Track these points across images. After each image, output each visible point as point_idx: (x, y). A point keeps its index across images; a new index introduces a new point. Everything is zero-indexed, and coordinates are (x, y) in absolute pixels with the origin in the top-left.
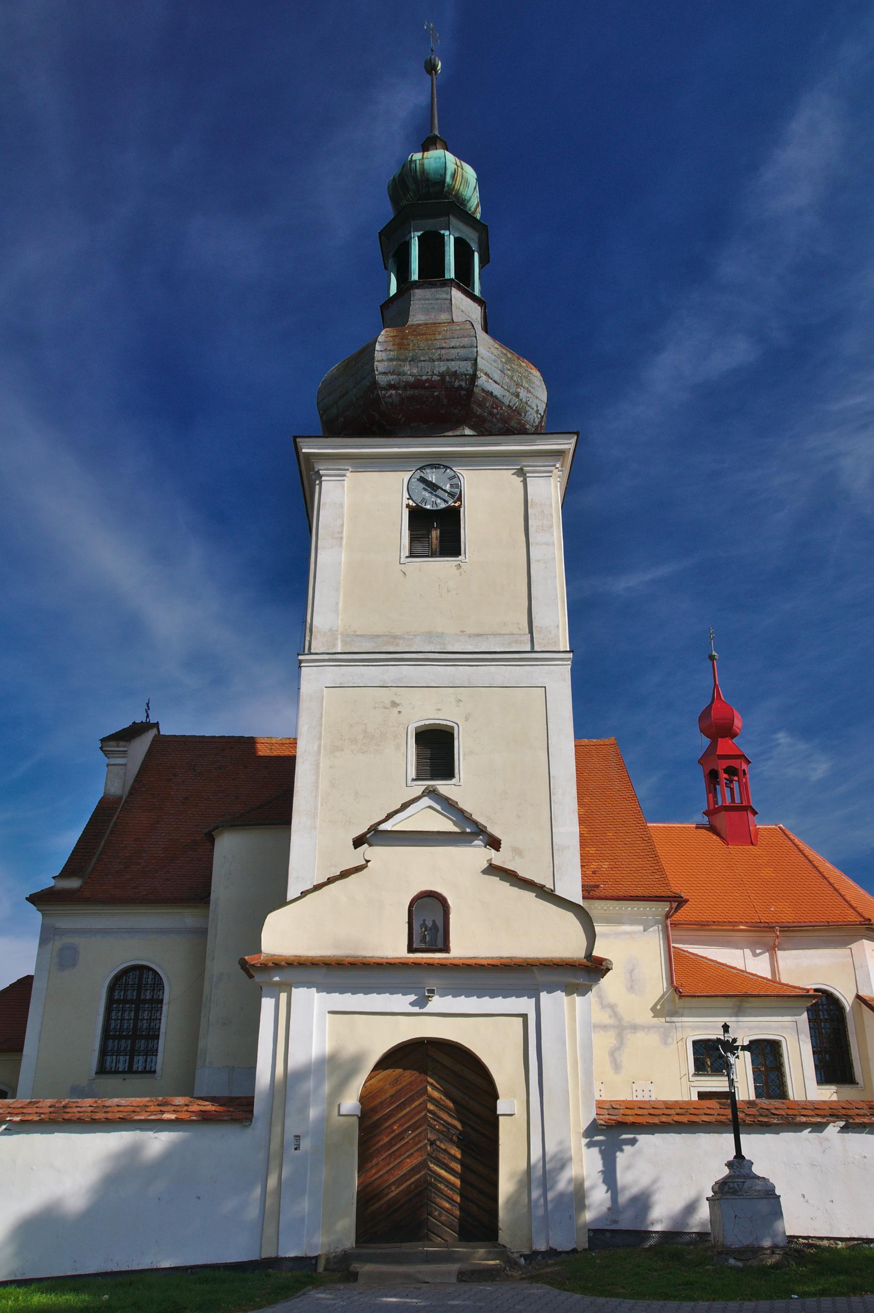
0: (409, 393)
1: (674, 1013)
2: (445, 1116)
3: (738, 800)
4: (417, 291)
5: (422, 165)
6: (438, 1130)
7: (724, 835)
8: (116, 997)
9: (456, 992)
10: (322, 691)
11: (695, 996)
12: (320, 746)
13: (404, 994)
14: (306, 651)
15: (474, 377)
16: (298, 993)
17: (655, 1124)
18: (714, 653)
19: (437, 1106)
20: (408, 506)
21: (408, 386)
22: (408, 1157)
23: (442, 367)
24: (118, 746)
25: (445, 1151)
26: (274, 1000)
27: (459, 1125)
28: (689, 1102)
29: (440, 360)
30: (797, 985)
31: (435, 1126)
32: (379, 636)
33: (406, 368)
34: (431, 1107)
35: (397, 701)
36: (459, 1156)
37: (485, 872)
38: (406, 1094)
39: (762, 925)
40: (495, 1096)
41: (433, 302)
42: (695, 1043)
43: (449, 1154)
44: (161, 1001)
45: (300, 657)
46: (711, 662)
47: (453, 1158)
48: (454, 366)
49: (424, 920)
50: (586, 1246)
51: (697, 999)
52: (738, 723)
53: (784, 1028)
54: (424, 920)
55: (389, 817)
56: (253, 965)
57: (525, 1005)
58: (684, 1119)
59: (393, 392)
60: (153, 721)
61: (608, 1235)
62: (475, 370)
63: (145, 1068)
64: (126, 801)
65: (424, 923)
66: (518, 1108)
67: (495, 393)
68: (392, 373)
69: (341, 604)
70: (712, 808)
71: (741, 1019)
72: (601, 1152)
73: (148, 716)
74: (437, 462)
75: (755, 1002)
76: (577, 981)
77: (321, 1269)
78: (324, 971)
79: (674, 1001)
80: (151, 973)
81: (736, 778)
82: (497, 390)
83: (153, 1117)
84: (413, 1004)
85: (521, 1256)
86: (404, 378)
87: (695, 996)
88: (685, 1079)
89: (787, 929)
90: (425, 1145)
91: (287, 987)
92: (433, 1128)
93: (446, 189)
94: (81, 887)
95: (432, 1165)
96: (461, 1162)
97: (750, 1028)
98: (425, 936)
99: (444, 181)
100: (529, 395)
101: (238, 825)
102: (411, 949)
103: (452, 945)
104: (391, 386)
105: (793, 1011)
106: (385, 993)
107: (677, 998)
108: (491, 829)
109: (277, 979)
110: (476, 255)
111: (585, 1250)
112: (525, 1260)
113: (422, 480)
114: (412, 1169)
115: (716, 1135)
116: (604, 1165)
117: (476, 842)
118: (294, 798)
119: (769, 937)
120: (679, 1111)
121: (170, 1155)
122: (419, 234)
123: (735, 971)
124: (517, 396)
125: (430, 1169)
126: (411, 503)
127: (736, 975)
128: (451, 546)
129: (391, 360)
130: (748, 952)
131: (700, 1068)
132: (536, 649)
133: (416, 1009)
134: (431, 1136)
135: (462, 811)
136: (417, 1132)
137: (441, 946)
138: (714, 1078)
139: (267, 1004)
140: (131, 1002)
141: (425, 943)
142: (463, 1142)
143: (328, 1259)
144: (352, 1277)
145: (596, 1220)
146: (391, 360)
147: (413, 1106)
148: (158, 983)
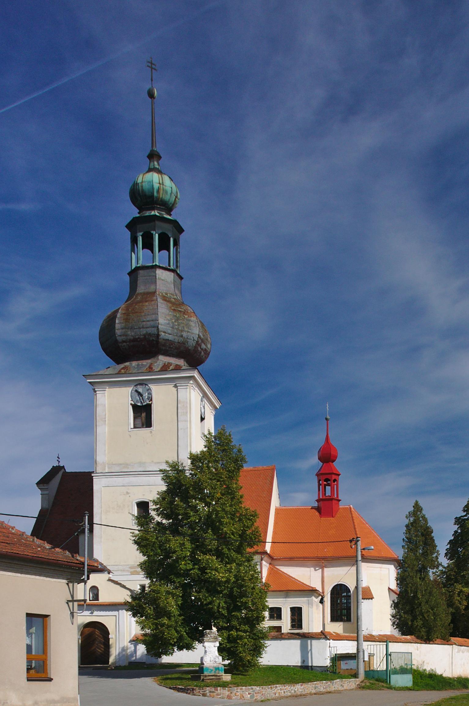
0: (132, 344)
3: (321, 497)
4: (140, 271)
5: (142, 186)
15: (158, 335)
20: (131, 404)
21: (131, 341)
23: (144, 331)
29: (143, 327)
32: (121, 464)
33: (129, 333)
40: (109, 634)
41: (148, 278)
46: (326, 421)
48: (150, 330)
59: (125, 344)
62: (158, 332)
67: (170, 339)
68: (124, 335)
69: (106, 452)
74: (142, 383)
75: (292, 593)
82: (170, 337)
86: (129, 338)
89: (325, 559)
93: (155, 199)
99: (153, 196)
100: (189, 334)
103: (100, 599)
104: (124, 342)
110: (172, 239)
113: (136, 391)
122: (141, 234)
124: (182, 336)
126: (133, 403)
128: (148, 423)
129: (122, 329)
130: (312, 569)
146: (122, 329)
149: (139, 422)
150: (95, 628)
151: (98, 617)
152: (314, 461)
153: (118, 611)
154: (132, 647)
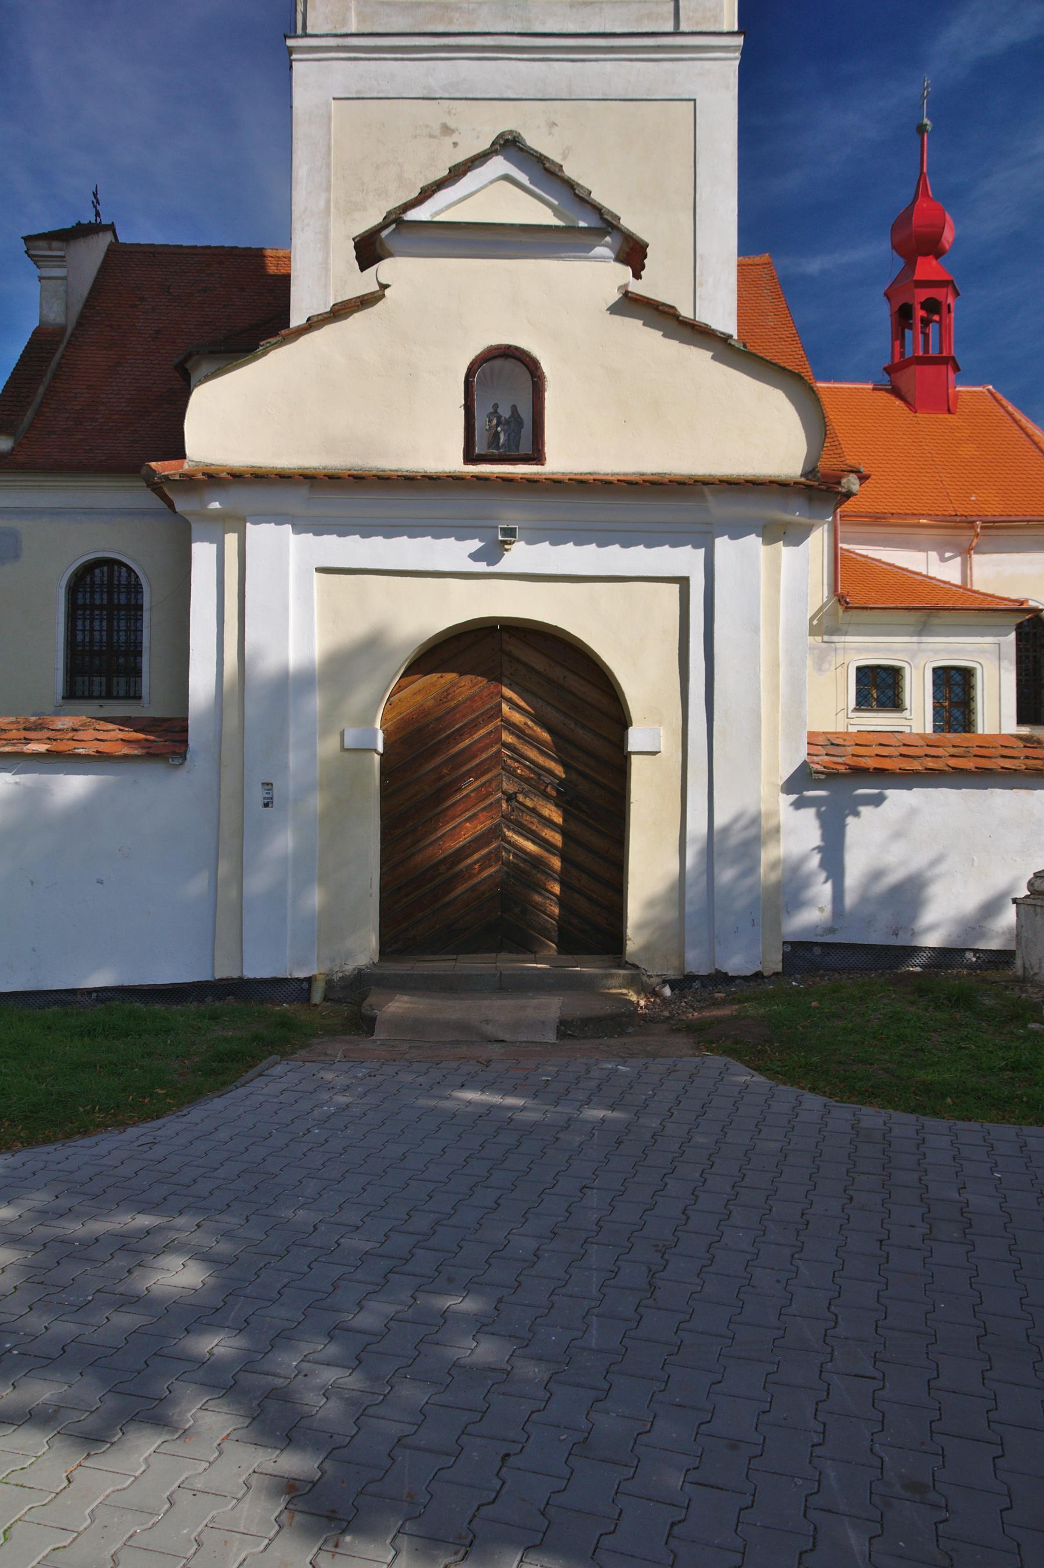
1: (834, 631)
2: (532, 754)
6: (520, 777)
7: (910, 400)
8: (80, 602)
9: (558, 535)
10: (328, 105)
11: (866, 608)
12: (328, 201)
13: (459, 538)
14: (299, 31)
16: (259, 534)
17: (915, 773)
18: (926, 121)
19: (518, 737)
22: (468, 820)
24: (50, 249)
25: (533, 811)
26: (214, 546)
27: (559, 770)
28: (922, 736)
30: (1006, 596)
31: (515, 770)
34: (507, 737)
35: (452, 124)
36: (558, 819)
37: (615, 309)
38: (464, 716)
39: (958, 519)
42: (859, 669)
43: (541, 816)
44: (140, 607)
45: (290, 43)
47: (549, 822)
49: (496, 406)
50: (779, 968)
51: (869, 612)
52: (948, 236)
53: (983, 652)
54: (496, 406)
55: (427, 193)
56: (166, 477)
57: (685, 560)
58: (970, 764)
60: (105, 221)
61: (817, 951)
63: (128, 692)
64: (73, 334)
65: (496, 412)
66: (668, 743)
70: (896, 361)
71: (925, 639)
72: (819, 815)
73: (97, 214)
76: (787, 517)
77: (317, 997)
78: (304, 492)
79: (836, 614)
80: (124, 570)
81: (936, 318)
83: (7, 749)
84: (475, 556)
85: (665, 982)
87: (866, 608)
88: (842, 715)
89: (992, 525)
90: (499, 800)
91: (237, 522)
92: (512, 773)
94: (13, 449)
95: (509, 834)
96: (563, 831)
97: (936, 652)
98: (496, 435)
101: (221, 352)
102: (470, 457)
105: (998, 630)
106: (423, 535)
107: (841, 611)
108: (628, 222)
109: (216, 505)
111: (776, 974)
112: (672, 989)
114: (476, 840)
115: (1022, 792)
116: (824, 837)
117: (599, 250)
118: (292, 289)
119: (965, 536)
120: (952, 751)
121: (85, 811)
123: (920, 578)
125: (505, 839)
127: (922, 583)
130: (933, 555)
131: (863, 702)
132: (684, 27)
133: (481, 567)
134: (508, 786)
135: (570, 185)
136: (484, 779)
137: (525, 448)
138: (881, 715)
139: (203, 554)
140: (101, 607)
141: (498, 447)
142: (566, 798)
143: (330, 984)
144: (365, 1024)
145: (807, 930)
147: (476, 737)
148: (135, 588)
149: (120, 684)
150: (496, 676)
151: (547, 583)
152: (876, 253)
153: (705, 541)
154: (799, 833)
